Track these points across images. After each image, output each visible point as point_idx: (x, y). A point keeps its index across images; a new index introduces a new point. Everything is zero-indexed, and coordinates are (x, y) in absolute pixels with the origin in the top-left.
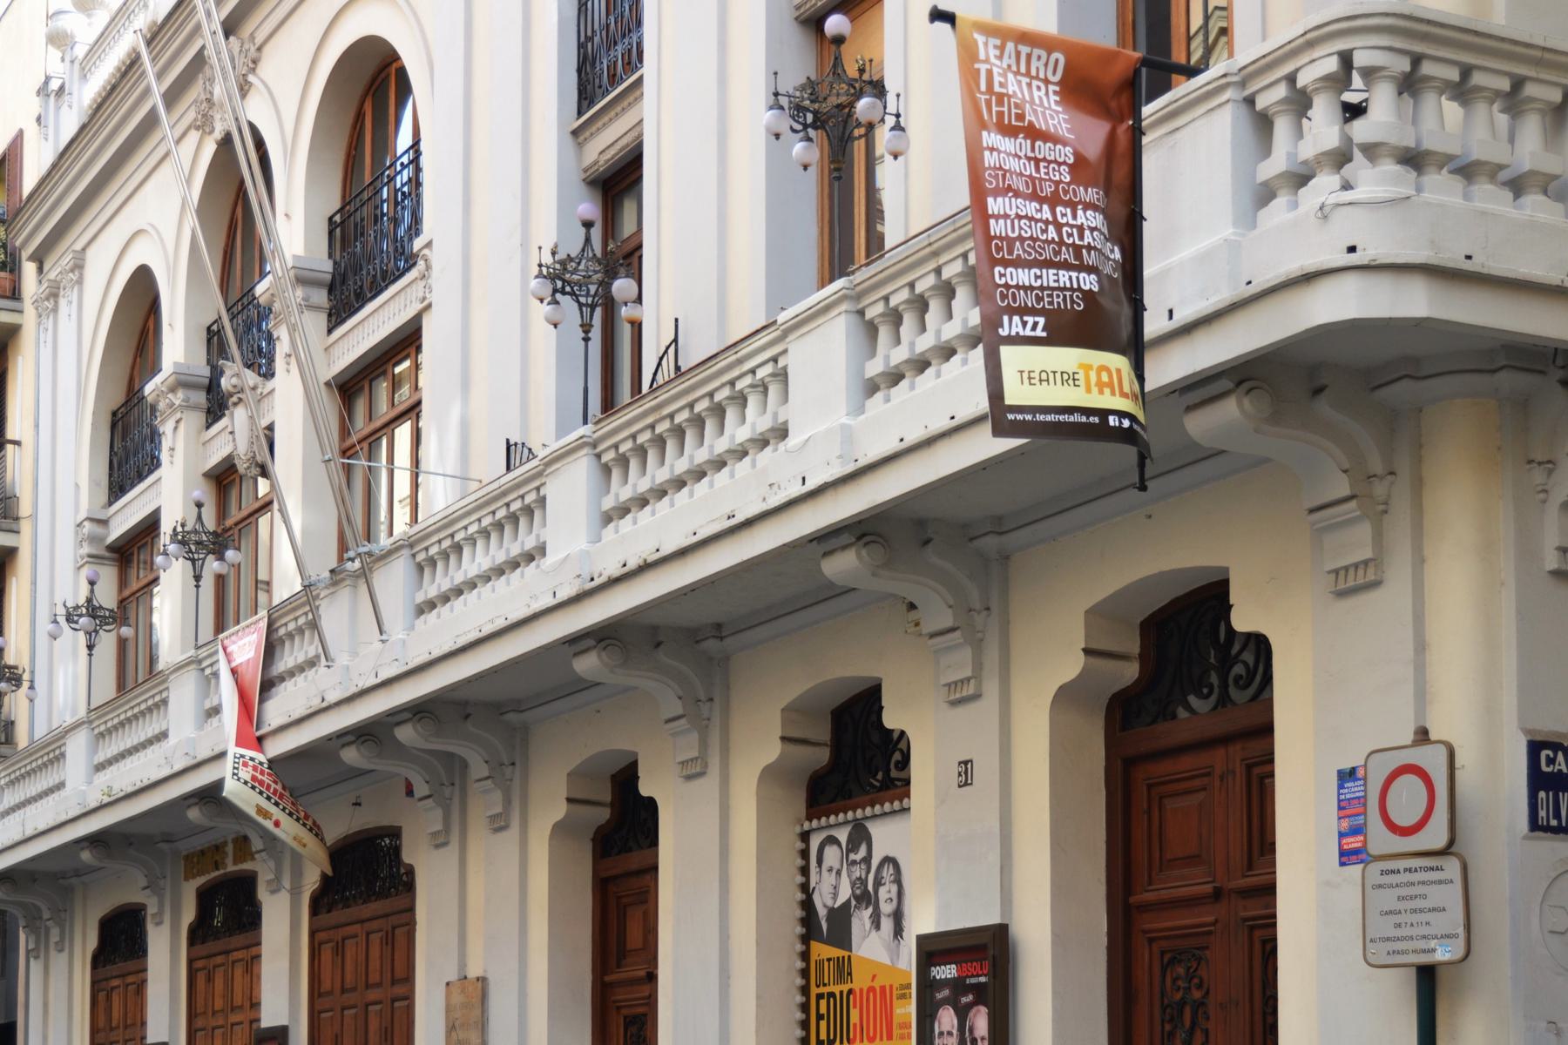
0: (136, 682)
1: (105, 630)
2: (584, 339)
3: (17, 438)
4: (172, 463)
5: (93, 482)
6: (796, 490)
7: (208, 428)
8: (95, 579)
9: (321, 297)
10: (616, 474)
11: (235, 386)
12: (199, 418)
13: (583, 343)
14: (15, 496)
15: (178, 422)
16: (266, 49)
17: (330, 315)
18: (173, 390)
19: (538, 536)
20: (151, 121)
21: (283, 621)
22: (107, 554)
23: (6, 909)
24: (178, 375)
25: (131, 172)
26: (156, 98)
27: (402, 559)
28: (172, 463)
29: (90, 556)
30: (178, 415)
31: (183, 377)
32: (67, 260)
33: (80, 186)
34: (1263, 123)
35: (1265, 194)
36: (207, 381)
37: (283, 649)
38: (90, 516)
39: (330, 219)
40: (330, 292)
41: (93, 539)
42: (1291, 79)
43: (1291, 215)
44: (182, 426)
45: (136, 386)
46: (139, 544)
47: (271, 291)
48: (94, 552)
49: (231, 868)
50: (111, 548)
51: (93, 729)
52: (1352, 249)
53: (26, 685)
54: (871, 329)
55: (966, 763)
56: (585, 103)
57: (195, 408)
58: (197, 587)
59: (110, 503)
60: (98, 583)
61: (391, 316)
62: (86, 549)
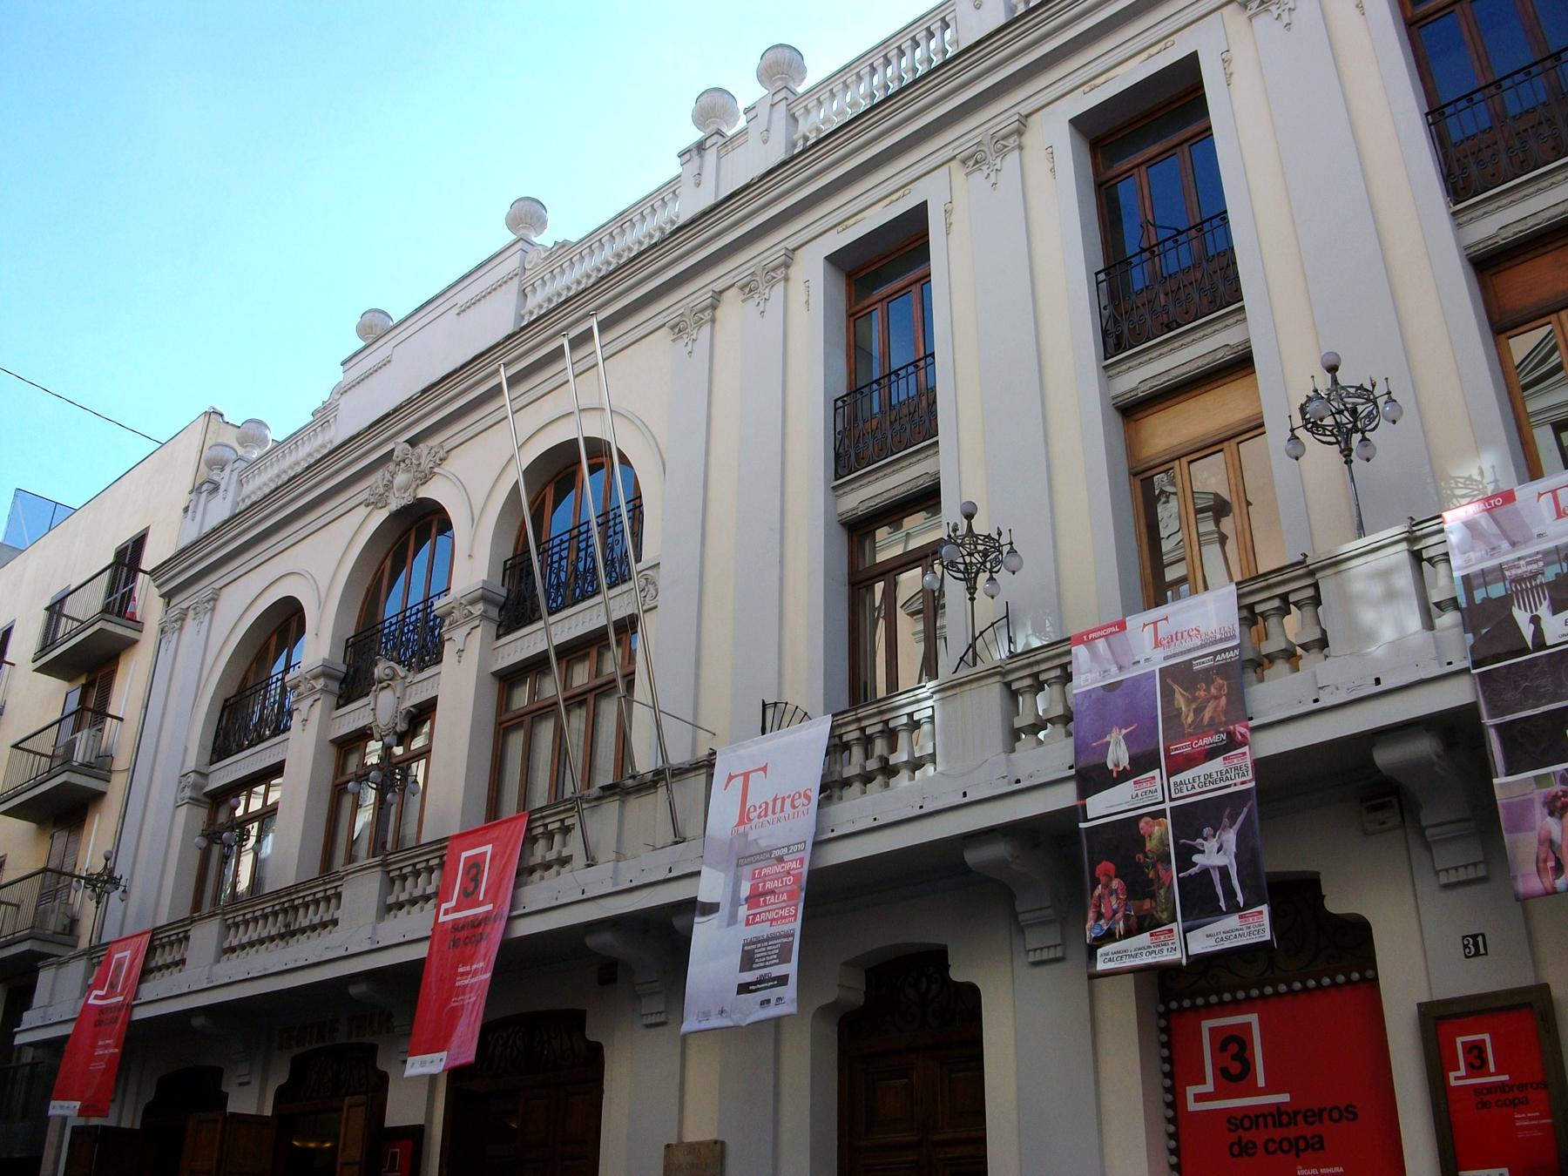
0: (397, 848)
1: (1369, 431)
2: (1346, 462)
3: (121, 716)
4: (459, 662)
5: (202, 747)
6: (186, 990)
7: (337, 709)
8: (974, 512)
9: (335, 686)
10: (233, 931)
11: (387, 675)
12: (334, 700)
13: (1346, 466)
14: (111, 756)
15: (315, 701)
16: (452, 453)
17: (499, 626)
18: (316, 677)
19: (183, 955)
20: (496, 391)
21: (160, 936)
22: (204, 799)
23: (1265, 886)
24: (327, 669)
25: (263, 550)
26: (503, 377)
27: (82, 961)
28: (459, 662)
29: (190, 798)
30: (317, 696)
31: (327, 669)
32: (206, 593)
33: (542, 350)
34: (1013, 695)
35: (1015, 735)
36: (503, 599)
37: (155, 954)
38: (198, 770)
39: (505, 562)
40: (500, 611)
41: (195, 787)
42: (562, 821)
43: (910, 783)
44: (319, 704)
45: (543, 538)
46: (346, 748)
47: (452, 605)
48: (194, 795)
49: (341, 1038)
50: (206, 794)
51: (92, 959)
52: (921, 807)
53: (121, 889)
54: (392, 881)
55: (1474, 937)
56: (215, 759)
57: (331, 692)
58: (972, 599)
59: (212, 763)
60: (1340, 368)
61: (519, 650)
62: (188, 793)
